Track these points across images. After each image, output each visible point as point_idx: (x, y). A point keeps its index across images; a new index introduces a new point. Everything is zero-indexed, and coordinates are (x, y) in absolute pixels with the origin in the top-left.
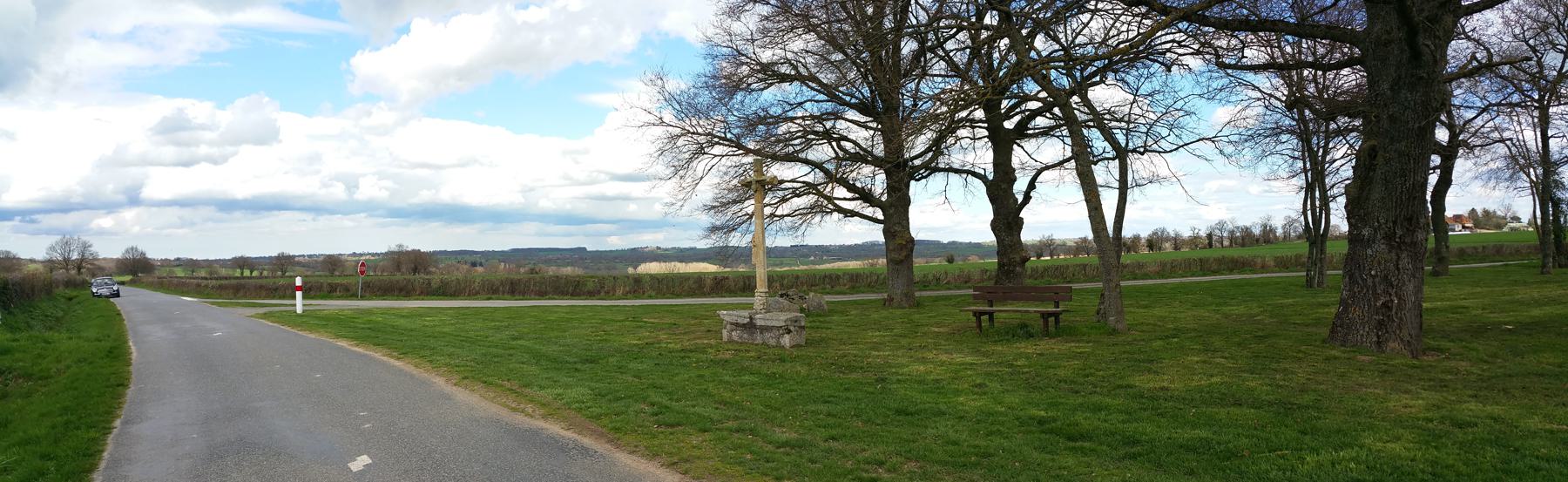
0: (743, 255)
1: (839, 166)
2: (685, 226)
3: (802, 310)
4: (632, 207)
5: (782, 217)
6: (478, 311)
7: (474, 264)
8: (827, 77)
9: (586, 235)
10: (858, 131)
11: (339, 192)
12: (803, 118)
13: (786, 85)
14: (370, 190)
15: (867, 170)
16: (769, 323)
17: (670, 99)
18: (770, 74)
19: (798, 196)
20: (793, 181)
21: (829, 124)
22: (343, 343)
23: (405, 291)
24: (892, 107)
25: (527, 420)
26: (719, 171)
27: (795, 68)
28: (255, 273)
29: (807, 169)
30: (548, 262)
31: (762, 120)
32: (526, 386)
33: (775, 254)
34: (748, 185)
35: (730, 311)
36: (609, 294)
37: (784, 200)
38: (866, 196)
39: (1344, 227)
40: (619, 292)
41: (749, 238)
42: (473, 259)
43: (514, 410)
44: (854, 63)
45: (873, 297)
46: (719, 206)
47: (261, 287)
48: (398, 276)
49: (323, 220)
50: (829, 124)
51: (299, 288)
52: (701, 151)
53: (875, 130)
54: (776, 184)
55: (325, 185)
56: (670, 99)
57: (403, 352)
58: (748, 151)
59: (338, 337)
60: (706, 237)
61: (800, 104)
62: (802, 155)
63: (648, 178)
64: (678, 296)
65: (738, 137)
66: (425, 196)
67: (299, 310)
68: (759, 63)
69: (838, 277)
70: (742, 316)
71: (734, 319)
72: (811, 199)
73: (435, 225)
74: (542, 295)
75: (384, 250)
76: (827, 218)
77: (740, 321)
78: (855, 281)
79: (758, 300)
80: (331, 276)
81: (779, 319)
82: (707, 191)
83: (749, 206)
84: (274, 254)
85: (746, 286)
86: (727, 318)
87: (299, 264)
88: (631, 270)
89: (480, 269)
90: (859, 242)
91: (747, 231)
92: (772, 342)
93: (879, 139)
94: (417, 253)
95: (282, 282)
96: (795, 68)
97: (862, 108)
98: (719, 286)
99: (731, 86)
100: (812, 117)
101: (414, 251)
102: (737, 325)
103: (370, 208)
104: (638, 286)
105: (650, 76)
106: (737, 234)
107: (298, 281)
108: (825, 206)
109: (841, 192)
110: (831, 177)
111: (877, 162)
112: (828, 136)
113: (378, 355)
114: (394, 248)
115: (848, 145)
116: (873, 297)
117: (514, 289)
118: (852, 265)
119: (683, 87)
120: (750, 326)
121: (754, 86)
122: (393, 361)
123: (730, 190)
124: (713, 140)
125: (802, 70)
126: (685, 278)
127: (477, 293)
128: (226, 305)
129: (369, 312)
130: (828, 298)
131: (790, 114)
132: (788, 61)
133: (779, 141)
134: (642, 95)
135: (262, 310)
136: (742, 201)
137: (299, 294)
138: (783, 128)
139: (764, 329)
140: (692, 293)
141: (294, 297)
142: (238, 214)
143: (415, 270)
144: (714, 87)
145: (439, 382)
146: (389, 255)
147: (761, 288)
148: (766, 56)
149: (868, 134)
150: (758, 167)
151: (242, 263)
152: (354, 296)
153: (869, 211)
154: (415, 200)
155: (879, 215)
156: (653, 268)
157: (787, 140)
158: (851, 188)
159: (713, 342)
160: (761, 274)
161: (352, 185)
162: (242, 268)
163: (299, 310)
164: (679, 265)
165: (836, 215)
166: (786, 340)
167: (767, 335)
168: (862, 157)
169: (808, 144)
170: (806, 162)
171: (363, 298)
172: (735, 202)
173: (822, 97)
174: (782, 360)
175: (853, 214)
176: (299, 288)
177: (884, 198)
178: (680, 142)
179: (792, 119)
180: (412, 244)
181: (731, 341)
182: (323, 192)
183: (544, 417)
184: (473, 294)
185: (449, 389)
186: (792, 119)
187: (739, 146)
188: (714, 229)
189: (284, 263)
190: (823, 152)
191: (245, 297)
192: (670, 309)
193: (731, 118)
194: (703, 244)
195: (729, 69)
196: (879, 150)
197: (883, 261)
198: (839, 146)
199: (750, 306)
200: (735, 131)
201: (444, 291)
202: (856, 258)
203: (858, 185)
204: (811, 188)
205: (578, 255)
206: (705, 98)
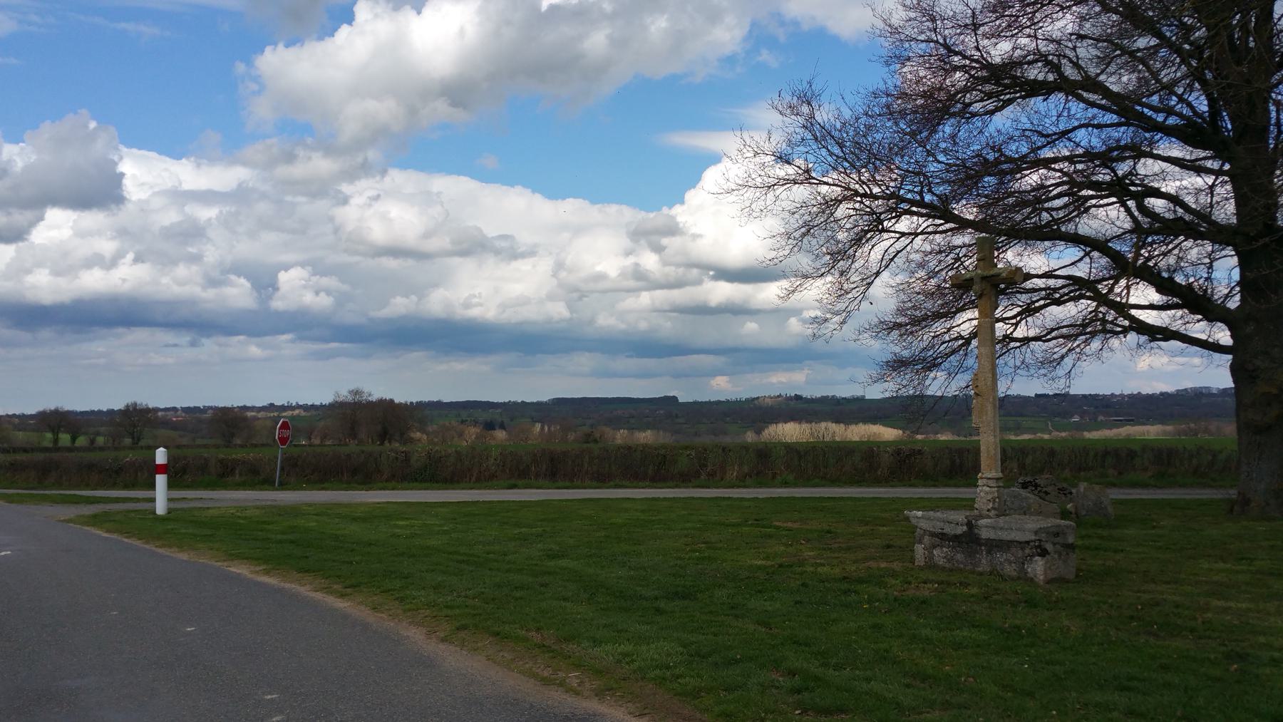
0: (955, 411)
1: (1137, 248)
2: (840, 358)
3: (1065, 515)
4: (751, 326)
5: (1026, 341)
6: (491, 508)
7: (490, 426)
8: (1120, 81)
9: (678, 375)
10: (1178, 178)
11: (239, 294)
12: (1070, 159)
13: (1037, 102)
14: (296, 287)
15: (1195, 251)
16: (1005, 536)
17: (820, 135)
18: (1005, 82)
19: (1058, 302)
20: (1047, 275)
21: (1123, 168)
22: (241, 570)
23: (362, 473)
24: (1253, 126)
25: (570, 700)
26: (903, 259)
27: (1056, 68)
28: (82, 441)
29: (1073, 253)
30: (616, 423)
31: (988, 167)
32: (568, 639)
33: (1014, 408)
34: (963, 285)
35: (929, 513)
36: (715, 478)
37: (1029, 311)
38: (1196, 301)
39: (649, 432)
40: (732, 474)
41: (962, 380)
42: (484, 416)
43: (546, 682)
44: (1178, 50)
45: (1216, 494)
46: (911, 321)
47: (91, 467)
48: (353, 447)
49: (209, 346)
50: (1123, 168)
51: (162, 469)
52: (876, 226)
53: (1217, 173)
54: (1017, 278)
55: (212, 282)
56: (820, 135)
57: (351, 585)
58: (963, 224)
59: (233, 557)
60: (881, 378)
61: (1064, 134)
62: (1068, 228)
63: (783, 275)
64: (834, 482)
65: (945, 200)
66: (400, 305)
67: (161, 508)
68: (989, 66)
69: (1132, 454)
70: (955, 521)
71: (938, 527)
72: (1086, 306)
73: (416, 355)
74: (602, 479)
75: (327, 399)
76: (1115, 342)
77: (948, 530)
78: (1163, 463)
79: (984, 491)
80: (222, 446)
81: (1025, 527)
82: (885, 295)
83: (966, 321)
84: (118, 405)
85: (961, 466)
86: (924, 525)
87: (166, 423)
88: (750, 437)
89: (500, 435)
90: (1169, 388)
91: (961, 368)
92: (1010, 570)
93: (1224, 189)
94: (387, 406)
95: (130, 456)
96: (1056, 68)
97: (1190, 133)
98: (903, 465)
99: (935, 109)
100: (1089, 155)
101: (382, 402)
102: (943, 537)
103: (301, 325)
104: (767, 464)
105: (788, 98)
106: (941, 375)
107: (161, 456)
108: (1111, 320)
109: (1143, 294)
110: (1125, 268)
111: (1219, 235)
112: (1119, 189)
113: (305, 589)
114: (344, 394)
115: (1157, 204)
116: (1216, 494)
117: (554, 468)
118: (1152, 432)
119: (847, 114)
120: (969, 540)
121: (977, 107)
122: (332, 601)
123: (930, 295)
124: (897, 205)
125: (1069, 71)
126: (845, 450)
127: (493, 477)
128: (20, 500)
129: (293, 511)
130: (1115, 494)
131: (1047, 153)
132: (1041, 57)
133: (1022, 204)
134: (772, 124)
135: (88, 510)
136: (950, 314)
137: (161, 480)
138: (1033, 179)
139: (996, 545)
140: (857, 479)
141: (152, 486)
142: (46, 333)
143: (384, 436)
144: (903, 114)
145: (415, 635)
146: (337, 408)
147: (989, 470)
148: (1000, 51)
149: (1199, 181)
150: (986, 252)
151: (55, 421)
152: (268, 483)
153: (1199, 329)
154: (385, 313)
155: (1223, 336)
156: (790, 432)
157: (1039, 196)
158: (1164, 285)
159: (897, 566)
160: (988, 443)
161: (265, 282)
162: (55, 430)
163: (161, 508)
164: (833, 427)
165: (1132, 337)
166: (1038, 568)
167: (1000, 557)
168: (1195, 225)
169: (1081, 207)
170: (1076, 239)
171: (283, 486)
172: (937, 316)
173: (1111, 118)
174: (1031, 603)
175: (1165, 334)
176: (162, 469)
177: (1234, 304)
178: (842, 211)
179: (1047, 163)
180: (377, 390)
181: (931, 566)
182: (211, 294)
183: (599, 694)
184: (484, 479)
185: (433, 648)
186: (1047, 163)
187: (948, 216)
188: (898, 365)
189: (136, 423)
190: (1108, 218)
191: (59, 485)
192: (818, 506)
193: (932, 167)
194: (877, 392)
195: (931, 80)
196: (1226, 212)
197: (1229, 429)
198: (1142, 209)
199: (969, 504)
200: (940, 190)
201: (435, 472)
202: (1162, 420)
203: (1179, 279)
204: (1081, 287)
205: (663, 411)
206: (886, 133)
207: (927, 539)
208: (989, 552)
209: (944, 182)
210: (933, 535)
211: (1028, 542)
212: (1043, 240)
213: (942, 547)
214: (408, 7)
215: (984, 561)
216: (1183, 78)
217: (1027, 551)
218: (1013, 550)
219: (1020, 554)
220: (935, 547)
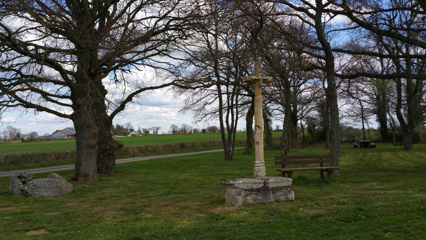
16: (279, 185)
71: (249, 186)
77: (255, 187)
86: (242, 186)
92: (283, 198)
139: (275, 190)
167: (279, 194)
207: (243, 193)
208: (273, 193)
209: (300, 96)
210: (246, 190)
211: (289, 186)
212: (422, 48)
213: (251, 195)
214: (380, 126)
215: (271, 197)
216: (268, 18)
217: (289, 189)
218: (283, 190)
219: (286, 191)
220: (247, 196)
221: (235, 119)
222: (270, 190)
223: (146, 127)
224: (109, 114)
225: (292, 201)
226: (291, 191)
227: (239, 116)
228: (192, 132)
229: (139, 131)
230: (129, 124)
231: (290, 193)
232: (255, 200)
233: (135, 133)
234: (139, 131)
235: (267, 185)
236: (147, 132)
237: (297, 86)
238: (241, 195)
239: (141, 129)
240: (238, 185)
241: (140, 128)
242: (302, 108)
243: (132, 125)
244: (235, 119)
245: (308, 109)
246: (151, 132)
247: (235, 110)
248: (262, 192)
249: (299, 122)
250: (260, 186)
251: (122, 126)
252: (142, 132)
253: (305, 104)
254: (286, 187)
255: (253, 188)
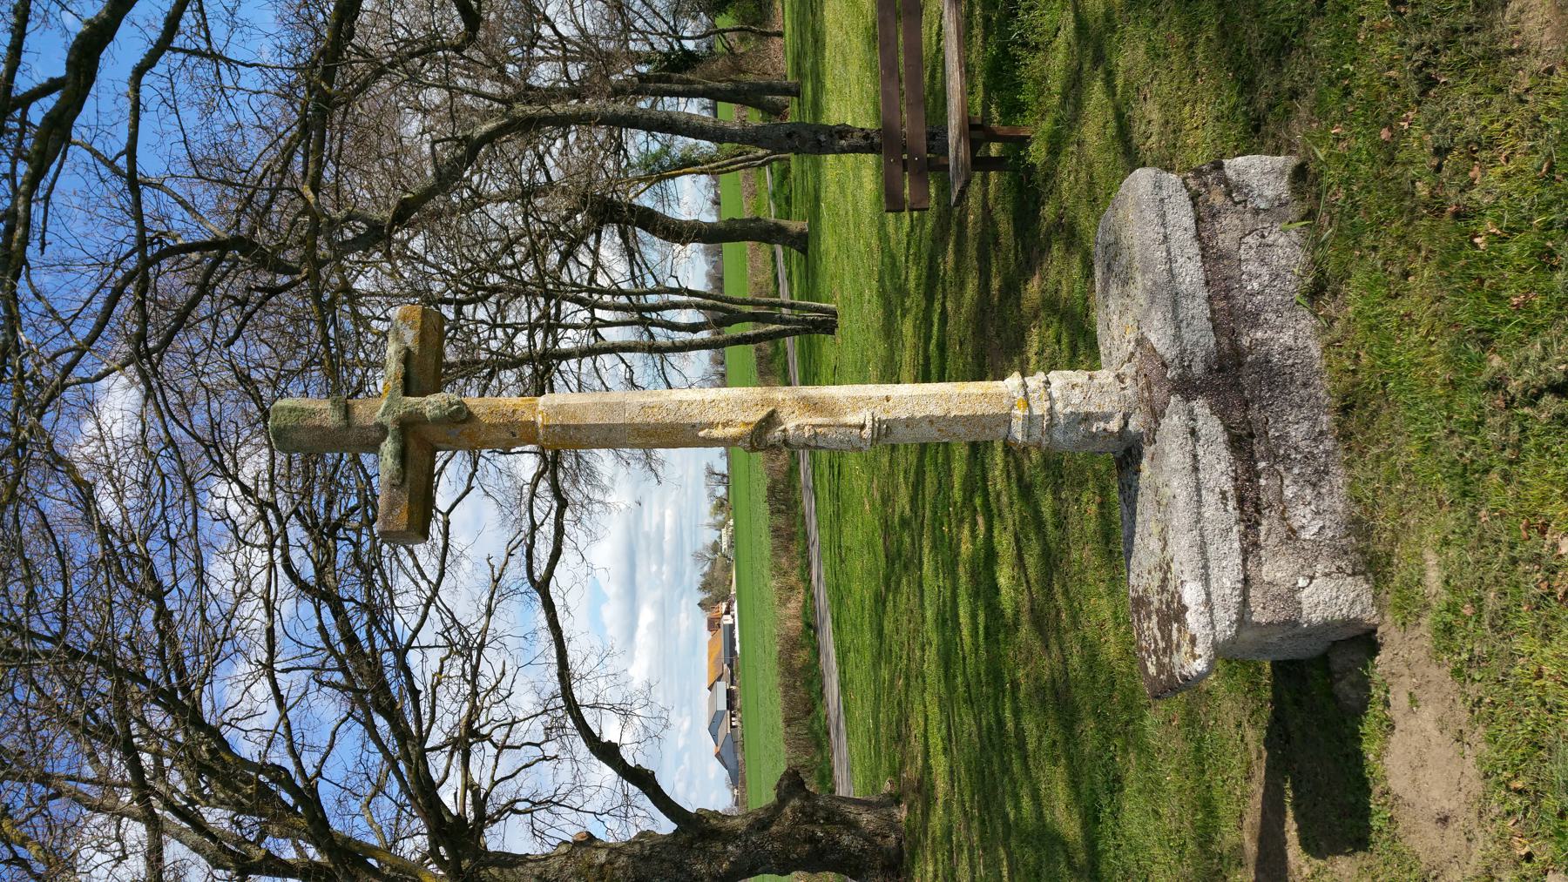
71: (1220, 515)
167: (1254, 277)
208: (1254, 319)
211: (1194, 198)
215: (1286, 338)
220: (1292, 534)
221: (685, 298)
222: (1234, 345)
223: (706, 507)
224: (666, 826)
225: (1300, 174)
226: (1225, 181)
227: (673, 284)
228: (721, 369)
229: (720, 526)
230: (698, 557)
231: (1239, 188)
232: (1323, 473)
233: (725, 539)
234: (720, 526)
235: (1198, 369)
236: (721, 505)
237: (565, 50)
238: (1294, 590)
239: (711, 520)
240: (1219, 613)
241: (709, 525)
242: (642, 32)
243: (700, 547)
244: (685, 298)
245: (646, 12)
246: (721, 491)
247: (653, 299)
248: (1253, 413)
249: (690, 45)
250: (1211, 426)
251: (704, 575)
252: (720, 518)
253: (628, 27)
254: (1198, 220)
255: (1228, 486)
